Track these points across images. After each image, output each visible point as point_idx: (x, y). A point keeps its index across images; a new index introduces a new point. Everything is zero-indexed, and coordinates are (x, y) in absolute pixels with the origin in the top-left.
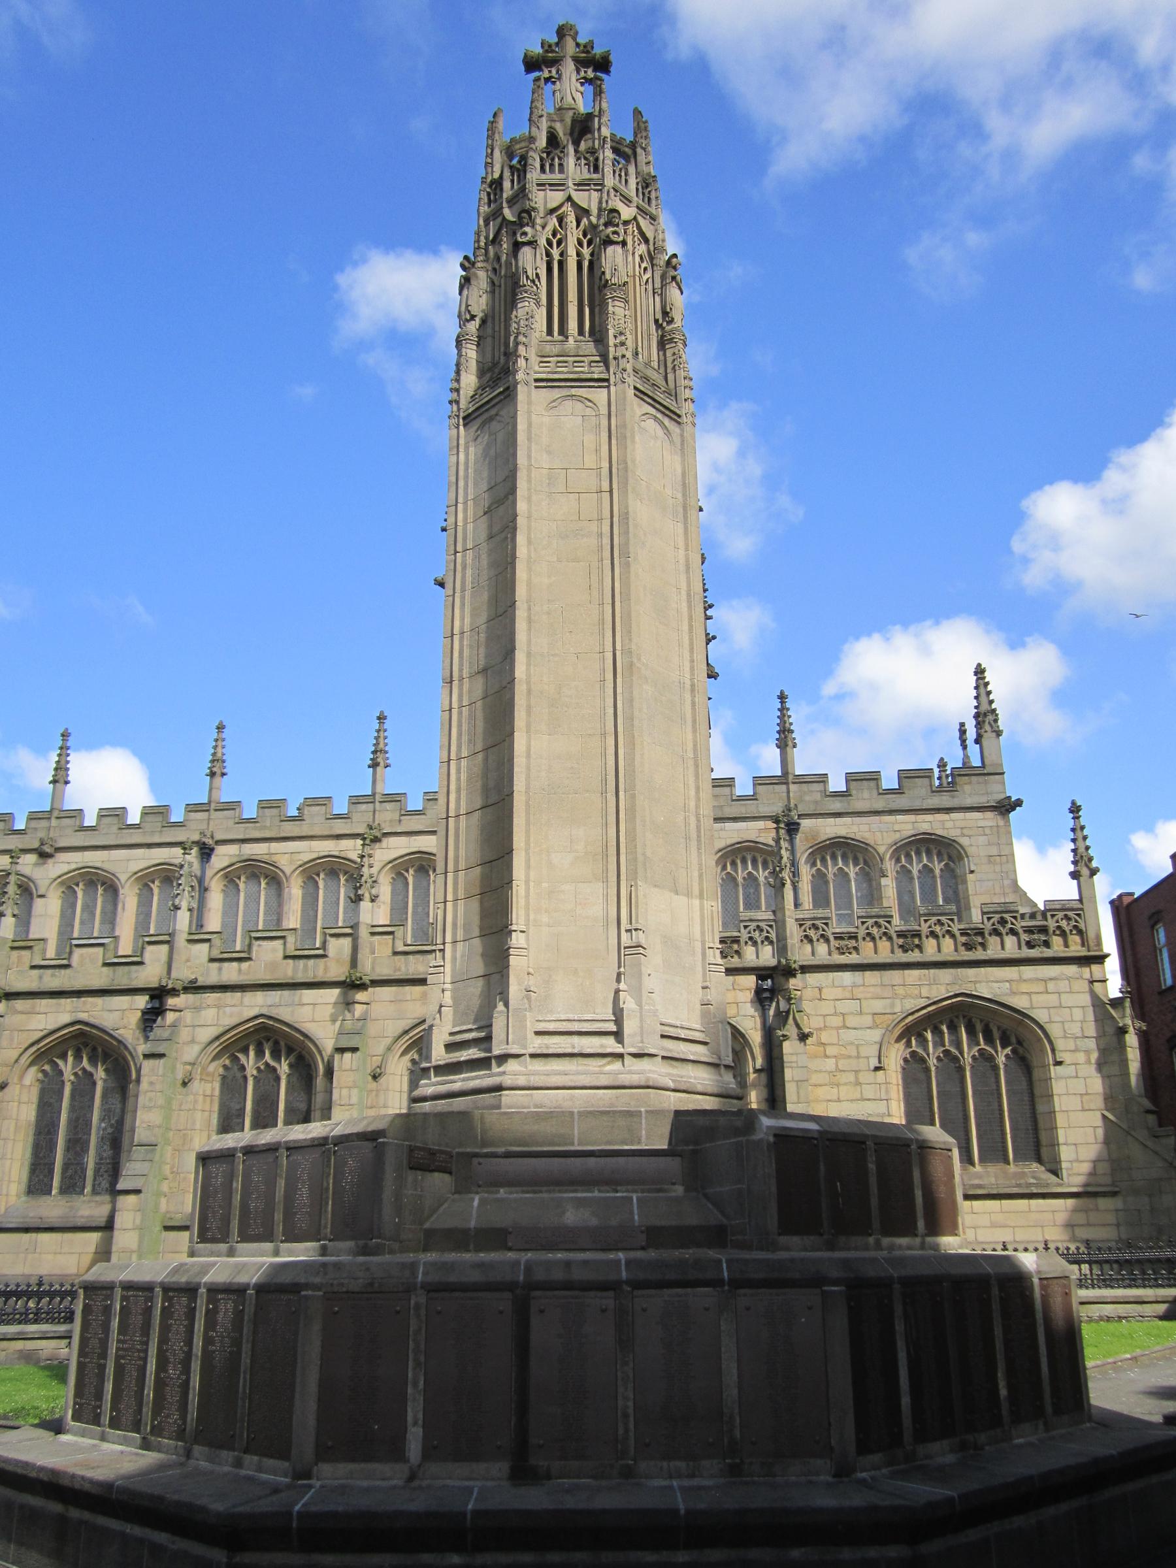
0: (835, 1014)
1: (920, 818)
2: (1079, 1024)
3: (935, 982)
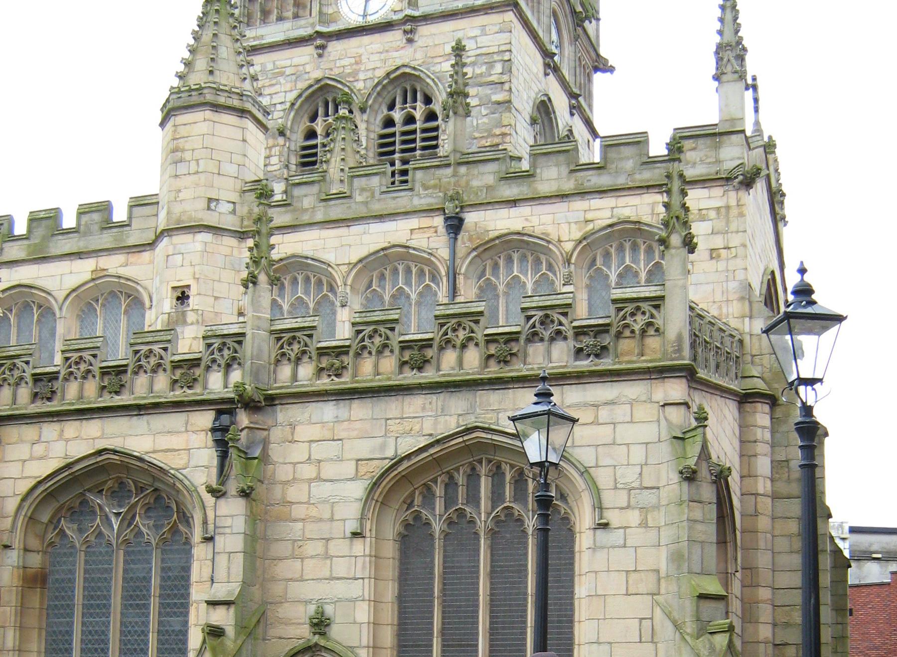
0: (67, 440)
1: (622, 201)
2: (638, 469)
3: (444, 412)
